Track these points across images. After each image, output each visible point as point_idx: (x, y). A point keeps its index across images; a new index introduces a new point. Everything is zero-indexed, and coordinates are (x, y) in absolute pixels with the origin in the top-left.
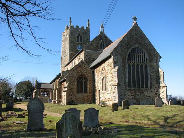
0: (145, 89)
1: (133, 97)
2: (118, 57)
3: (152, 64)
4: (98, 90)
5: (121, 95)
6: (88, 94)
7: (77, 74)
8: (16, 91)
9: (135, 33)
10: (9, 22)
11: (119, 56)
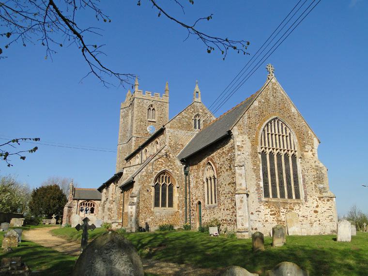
0: (296, 201)
1: (274, 218)
2: (243, 138)
3: (305, 154)
4: (196, 202)
5: (252, 213)
6: (177, 210)
7: (155, 171)
8: (30, 203)
9: (273, 95)
10: (46, 32)
11: (246, 137)
